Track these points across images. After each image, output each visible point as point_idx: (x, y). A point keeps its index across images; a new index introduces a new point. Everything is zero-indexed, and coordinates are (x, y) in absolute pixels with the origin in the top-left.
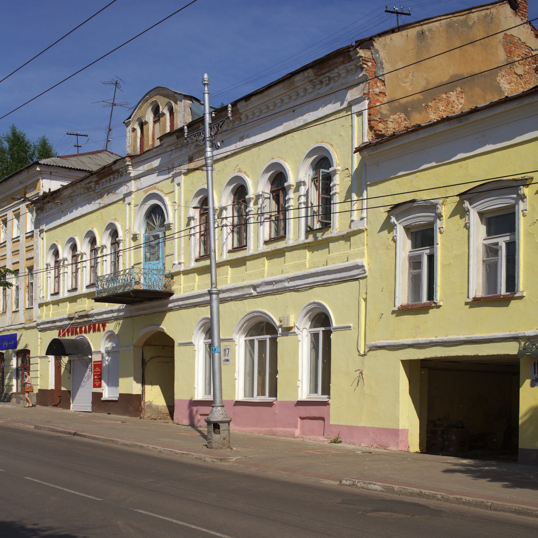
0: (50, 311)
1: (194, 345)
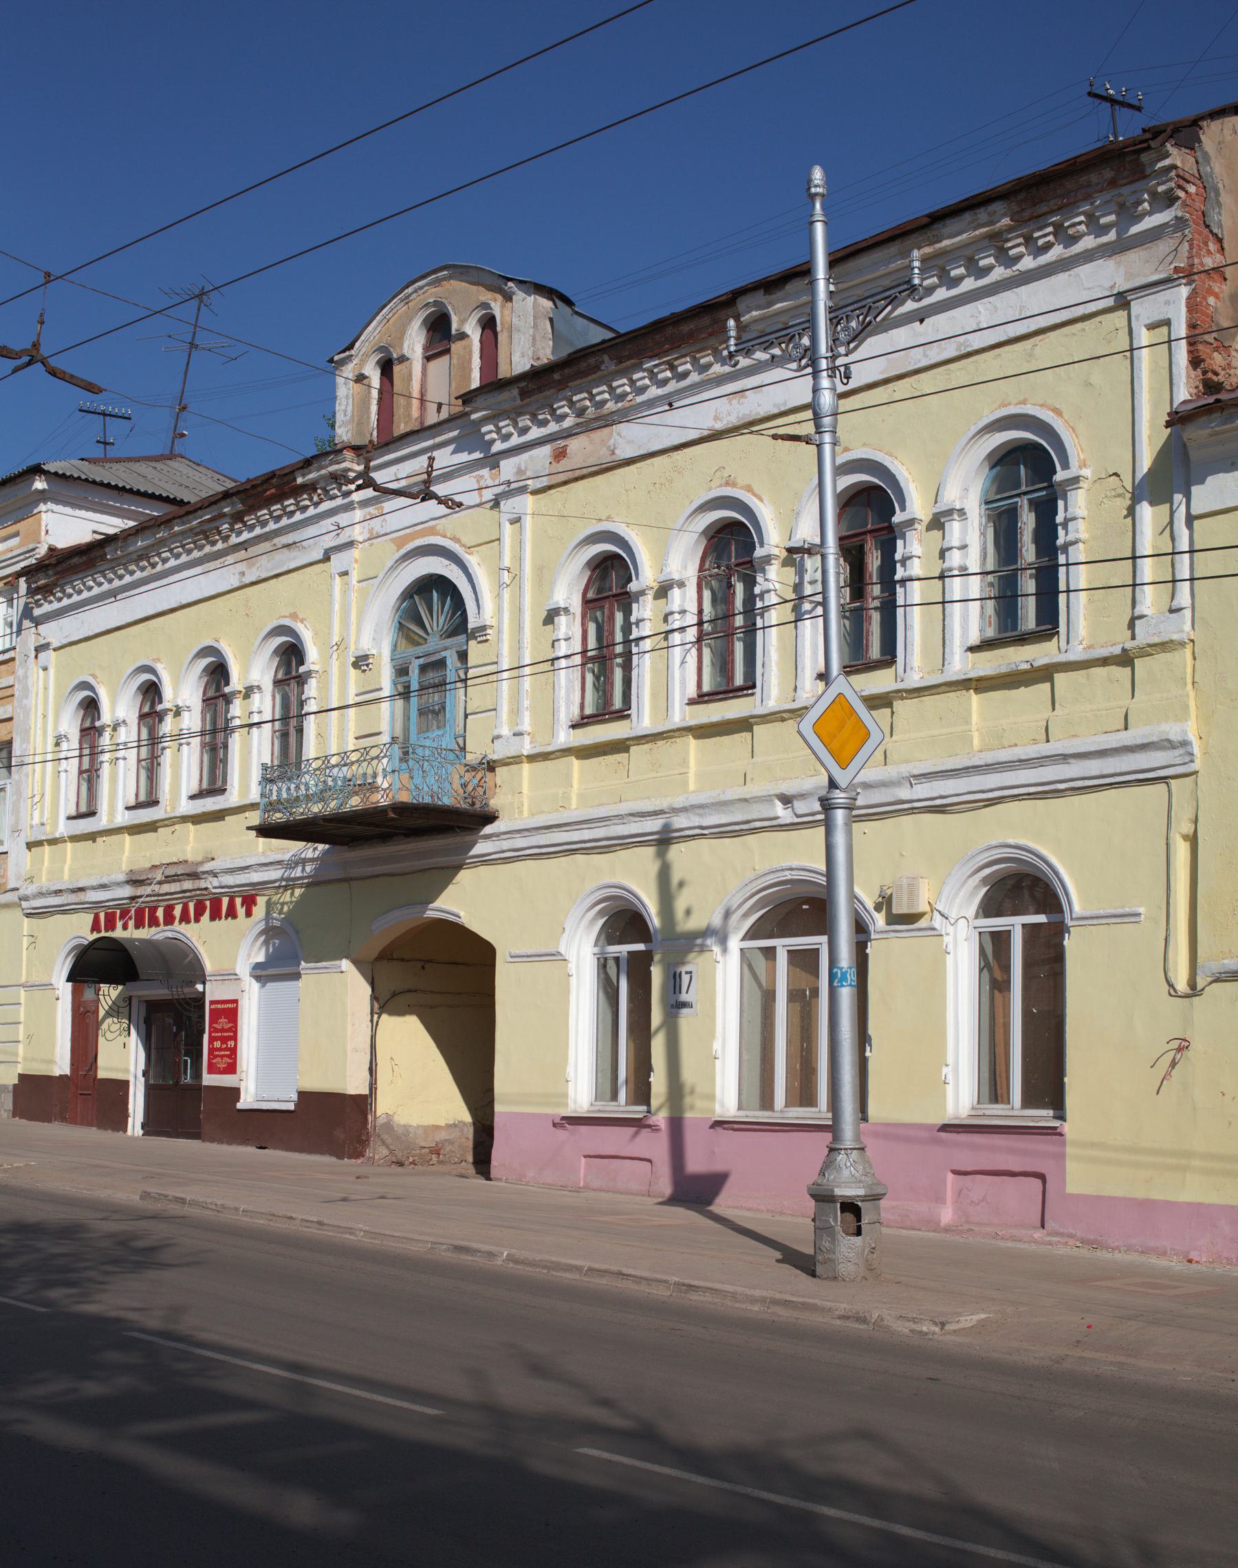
1: (565, 960)
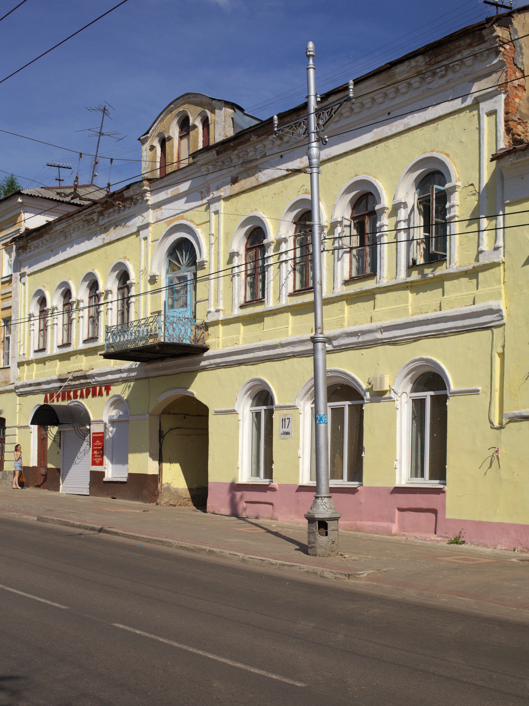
0: (33, 371)
1: (237, 413)
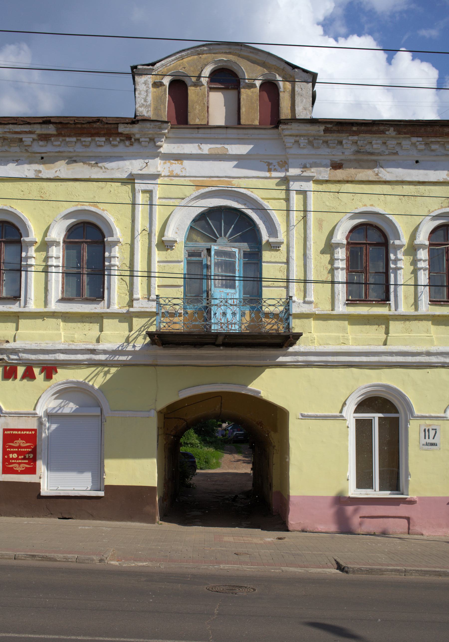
1: (346, 420)
